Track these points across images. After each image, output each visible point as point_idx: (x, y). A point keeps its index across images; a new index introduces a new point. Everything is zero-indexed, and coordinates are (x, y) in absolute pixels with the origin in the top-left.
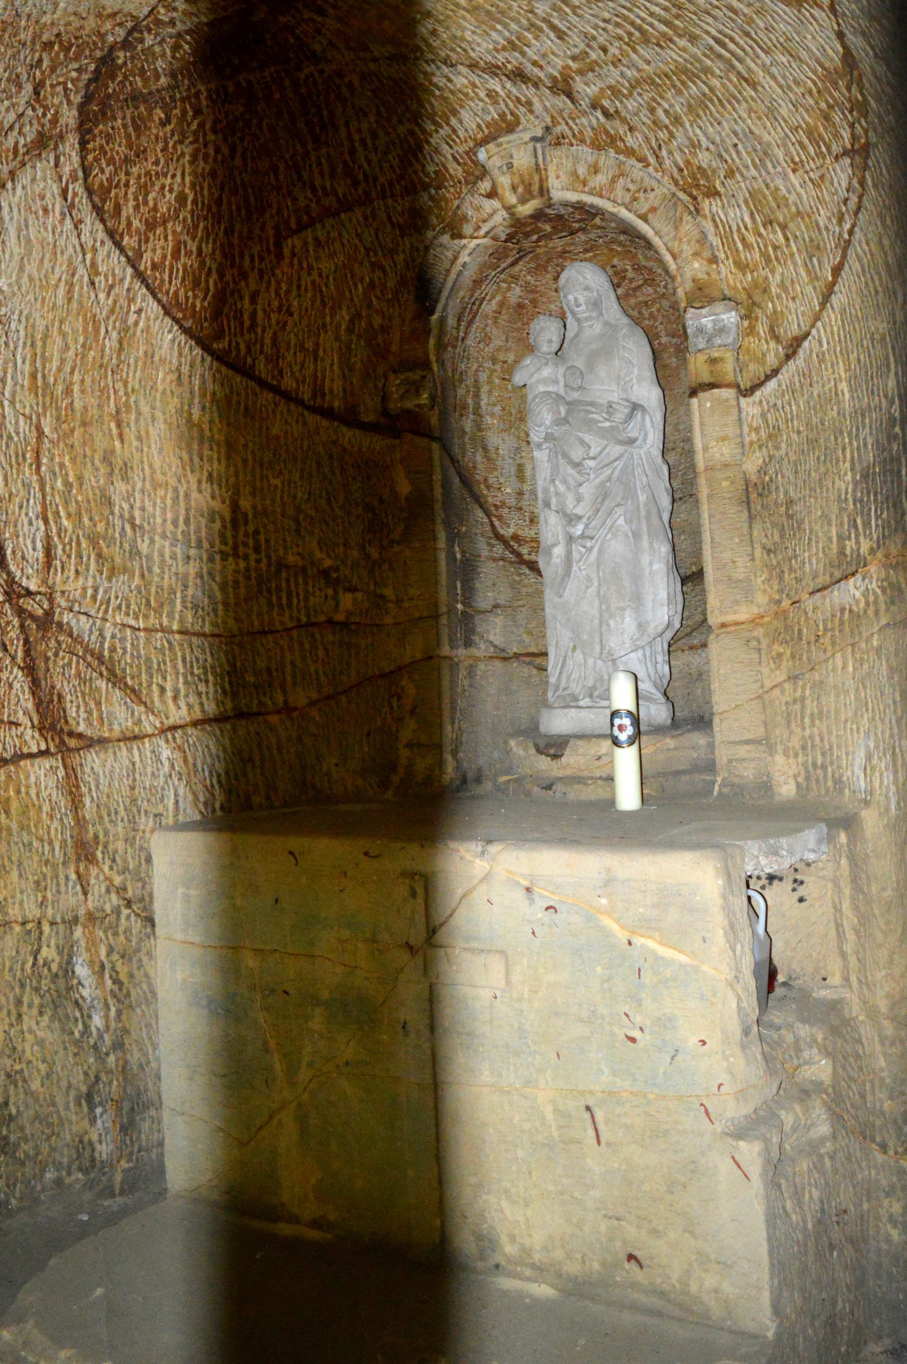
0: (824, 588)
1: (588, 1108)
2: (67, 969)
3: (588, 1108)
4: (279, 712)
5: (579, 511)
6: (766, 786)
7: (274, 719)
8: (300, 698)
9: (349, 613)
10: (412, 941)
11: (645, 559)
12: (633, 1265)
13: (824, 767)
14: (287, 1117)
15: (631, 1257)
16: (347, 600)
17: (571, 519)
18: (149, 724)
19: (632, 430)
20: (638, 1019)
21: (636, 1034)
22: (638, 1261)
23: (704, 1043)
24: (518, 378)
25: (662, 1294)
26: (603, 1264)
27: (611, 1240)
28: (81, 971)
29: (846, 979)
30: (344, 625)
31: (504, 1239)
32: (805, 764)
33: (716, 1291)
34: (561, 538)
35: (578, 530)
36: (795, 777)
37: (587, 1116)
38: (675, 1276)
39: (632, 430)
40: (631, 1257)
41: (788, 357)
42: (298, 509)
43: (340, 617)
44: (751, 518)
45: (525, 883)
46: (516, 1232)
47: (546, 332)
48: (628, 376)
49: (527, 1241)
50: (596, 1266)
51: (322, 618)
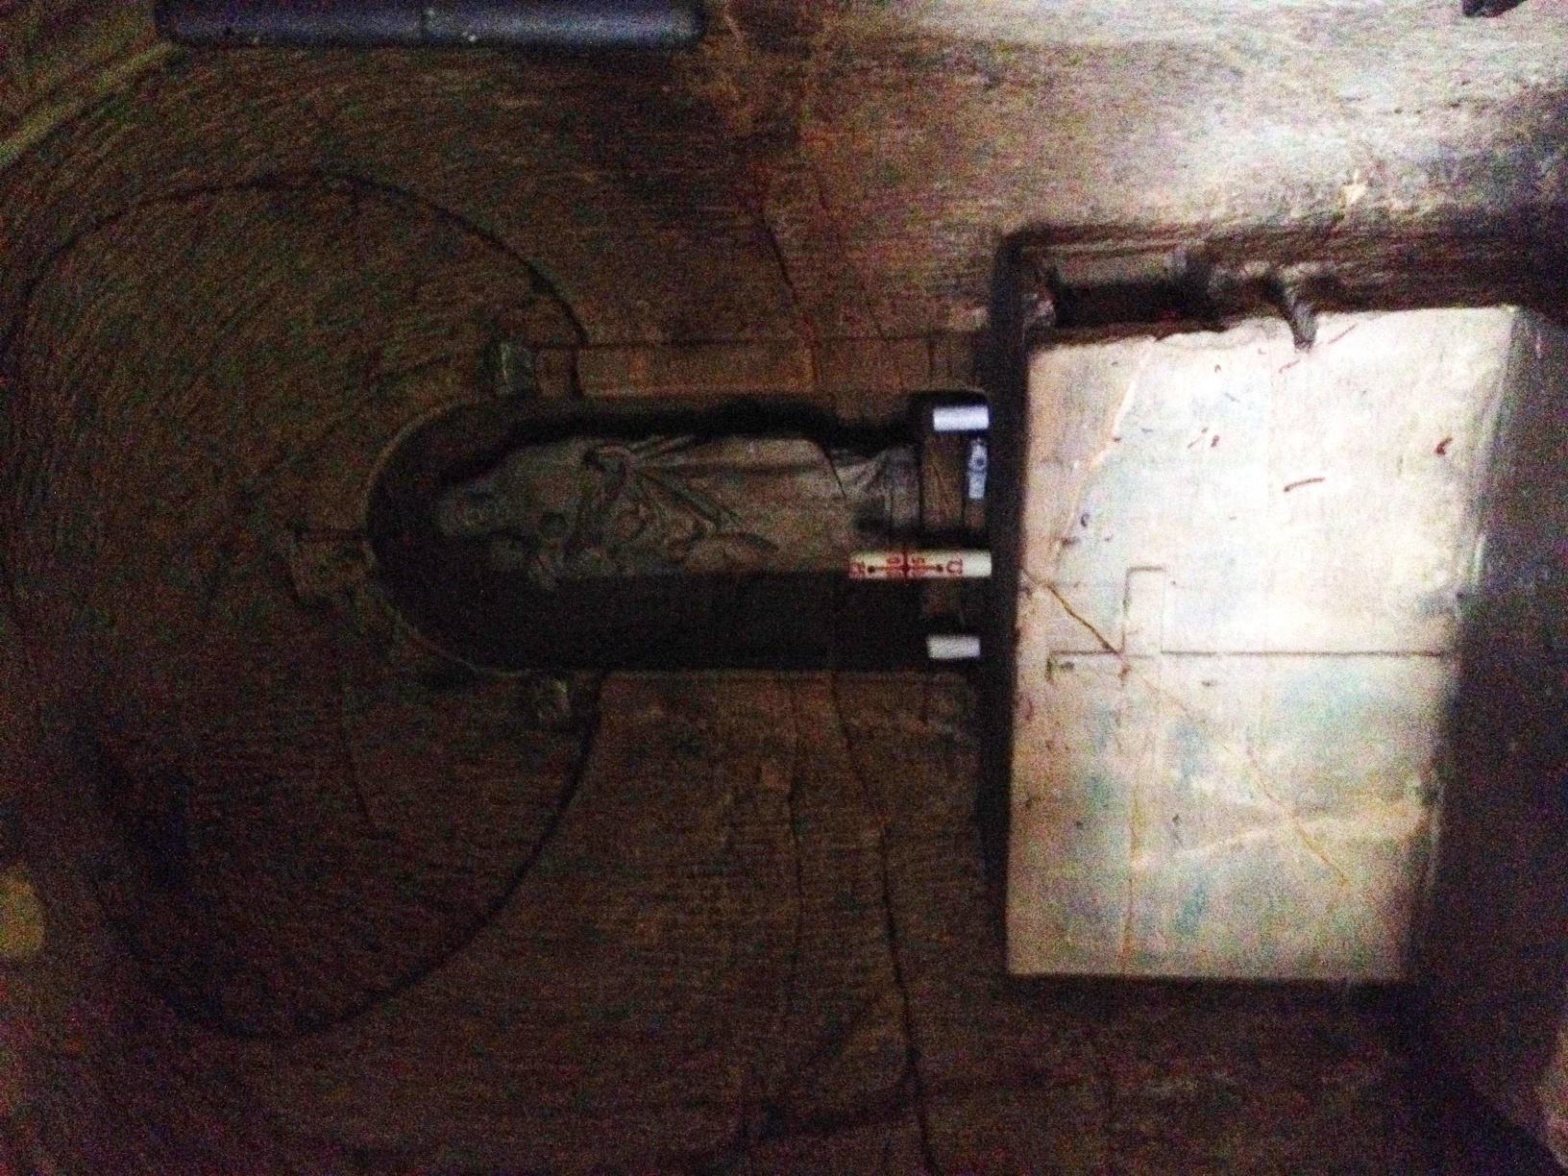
0: (783, 267)
1: (1287, 489)
2: (1166, 1106)
3: (1287, 489)
4: (885, 857)
5: (690, 524)
6: (974, 338)
7: (893, 863)
8: (869, 836)
9: (782, 779)
10: (1119, 670)
11: (740, 459)
12: (1450, 449)
13: (958, 276)
14: (1310, 827)
15: (1440, 450)
16: (770, 780)
17: (699, 534)
18: (893, 1000)
19: (613, 465)
20: (1195, 433)
21: (1209, 437)
22: (1442, 444)
23: (1218, 367)
24: (548, 584)
25: (1478, 419)
26: (1447, 480)
27: (1422, 470)
28: (1166, 1089)
29: (1166, 249)
30: (796, 783)
31: (1429, 586)
32: (956, 298)
33: (1470, 364)
34: (716, 544)
35: (709, 525)
36: (967, 308)
37: (1294, 492)
38: (1455, 404)
39: (613, 465)
40: (1440, 450)
41: (552, 291)
42: (668, 829)
43: (787, 788)
44: (708, 342)
45: (1057, 546)
46: (1420, 572)
47: (506, 555)
48: (557, 473)
49: (1432, 562)
50: (1451, 487)
51: (786, 809)
